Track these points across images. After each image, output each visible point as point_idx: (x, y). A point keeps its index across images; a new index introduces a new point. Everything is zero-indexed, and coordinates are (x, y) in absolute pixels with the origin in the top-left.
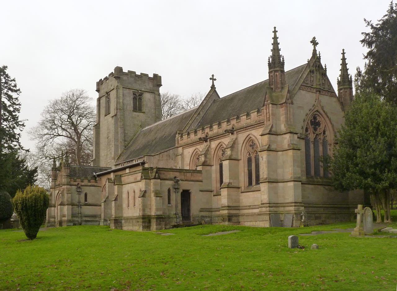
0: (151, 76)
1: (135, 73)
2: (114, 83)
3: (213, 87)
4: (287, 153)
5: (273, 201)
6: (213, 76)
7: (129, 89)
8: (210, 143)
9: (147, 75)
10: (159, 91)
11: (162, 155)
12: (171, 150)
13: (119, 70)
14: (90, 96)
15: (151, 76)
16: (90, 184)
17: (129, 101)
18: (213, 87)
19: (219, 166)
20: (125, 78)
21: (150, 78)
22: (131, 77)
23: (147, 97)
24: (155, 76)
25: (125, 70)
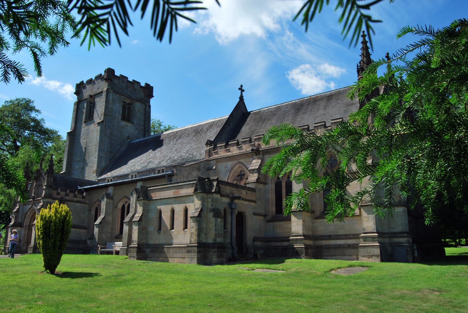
0: (143, 84)
1: (127, 78)
2: (104, 86)
3: (241, 98)
4: (134, 257)
5: (386, 230)
6: (242, 86)
7: (120, 94)
8: (263, 157)
9: (139, 83)
10: (149, 103)
11: (193, 167)
12: (202, 163)
13: (110, 72)
14: (37, 108)
15: (143, 84)
16: (76, 199)
17: (118, 108)
18: (241, 98)
19: (274, 185)
20: (116, 81)
21: (141, 87)
22: (123, 82)
23: (138, 106)
24: (147, 85)
25: (117, 74)
